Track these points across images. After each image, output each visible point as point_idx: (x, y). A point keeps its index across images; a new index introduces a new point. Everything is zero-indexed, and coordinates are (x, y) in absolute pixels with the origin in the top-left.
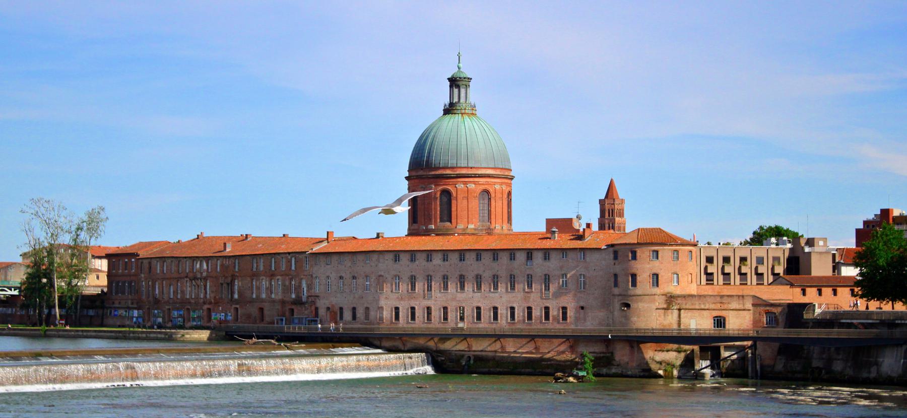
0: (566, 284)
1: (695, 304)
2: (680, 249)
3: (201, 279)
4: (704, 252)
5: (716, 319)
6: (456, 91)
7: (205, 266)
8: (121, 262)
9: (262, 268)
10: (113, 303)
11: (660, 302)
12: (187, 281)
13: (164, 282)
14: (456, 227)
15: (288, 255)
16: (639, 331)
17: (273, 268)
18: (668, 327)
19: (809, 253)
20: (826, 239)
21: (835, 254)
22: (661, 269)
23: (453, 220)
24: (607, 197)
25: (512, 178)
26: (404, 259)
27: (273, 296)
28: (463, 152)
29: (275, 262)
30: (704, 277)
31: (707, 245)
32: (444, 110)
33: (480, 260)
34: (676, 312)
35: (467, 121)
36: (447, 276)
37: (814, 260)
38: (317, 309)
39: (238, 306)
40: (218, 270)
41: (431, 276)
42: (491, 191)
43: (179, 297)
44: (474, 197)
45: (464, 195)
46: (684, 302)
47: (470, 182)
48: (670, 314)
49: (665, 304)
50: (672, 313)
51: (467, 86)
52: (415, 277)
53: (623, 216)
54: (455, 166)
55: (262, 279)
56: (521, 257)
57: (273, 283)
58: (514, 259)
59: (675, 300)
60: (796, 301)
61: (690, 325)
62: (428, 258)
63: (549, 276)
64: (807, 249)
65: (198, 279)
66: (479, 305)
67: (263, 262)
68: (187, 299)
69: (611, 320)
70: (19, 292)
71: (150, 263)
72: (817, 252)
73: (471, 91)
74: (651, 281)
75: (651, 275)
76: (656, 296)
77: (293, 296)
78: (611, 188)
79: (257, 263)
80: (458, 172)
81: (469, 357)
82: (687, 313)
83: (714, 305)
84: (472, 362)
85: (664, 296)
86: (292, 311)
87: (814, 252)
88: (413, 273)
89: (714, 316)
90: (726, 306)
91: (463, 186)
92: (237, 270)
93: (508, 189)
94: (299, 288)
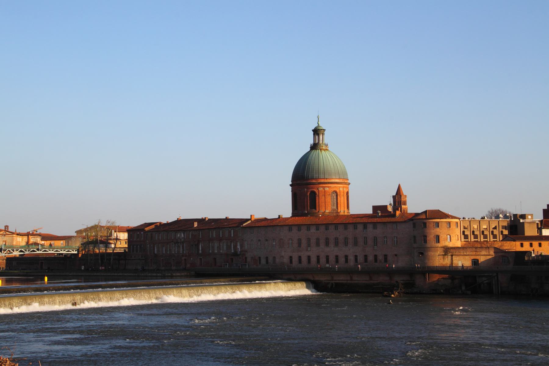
0: (386, 242)
1: (461, 253)
2: (451, 221)
3: (180, 243)
4: (462, 223)
5: (473, 260)
6: (317, 137)
7: (183, 236)
8: (135, 234)
9: (214, 236)
10: (131, 257)
11: (440, 252)
12: (172, 244)
13: (160, 245)
14: (325, 212)
15: (229, 228)
16: (429, 268)
17: (221, 236)
18: (446, 266)
19: (523, 223)
20: (532, 214)
21: (538, 223)
22: (441, 233)
23: (317, 208)
24: (397, 194)
25: (349, 184)
26: (295, 229)
27: (221, 251)
28: (322, 170)
29: (222, 232)
30: (463, 236)
31: (473, 219)
32: (311, 147)
33: (337, 229)
34: (450, 257)
35: (324, 153)
36: (319, 239)
37: (526, 226)
38: (246, 258)
39: (201, 257)
40: (190, 237)
41: (310, 239)
42: (338, 191)
43: (168, 253)
44: (328, 195)
45: (323, 194)
46: (454, 251)
47: (326, 187)
48: (446, 259)
49: (443, 252)
50: (448, 257)
51: (323, 134)
52: (301, 239)
53: (406, 205)
54: (318, 178)
55: (215, 242)
56: (360, 227)
57: (221, 244)
58: (356, 228)
59: (449, 250)
60: (518, 250)
61: (458, 264)
62: (308, 229)
63: (376, 237)
64: (521, 221)
65: (179, 243)
66: (338, 254)
67: (215, 233)
68: (173, 254)
69: (413, 262)
70: (77, 252)
71: (152, 234)
72: (528, 222)
73: (325, 136)
74: (435, 239)
75: (435, 236)
76: (438, 248)
77: (233, 251)
78: (399, 186)
79: (212, 233)
80: (319, 182)
81: (332, 284)
82: (456, 257)
83: (472, 252)
84: (334, 286)
85: (443, 248)
86: (232, 259)
87: (526, 222)
88: (300, 237)
89: (473, 259)
90: (479, 253)
91: (322, 189)
92: (201, 237)
93: (347, 190)
94: (235, 247)
